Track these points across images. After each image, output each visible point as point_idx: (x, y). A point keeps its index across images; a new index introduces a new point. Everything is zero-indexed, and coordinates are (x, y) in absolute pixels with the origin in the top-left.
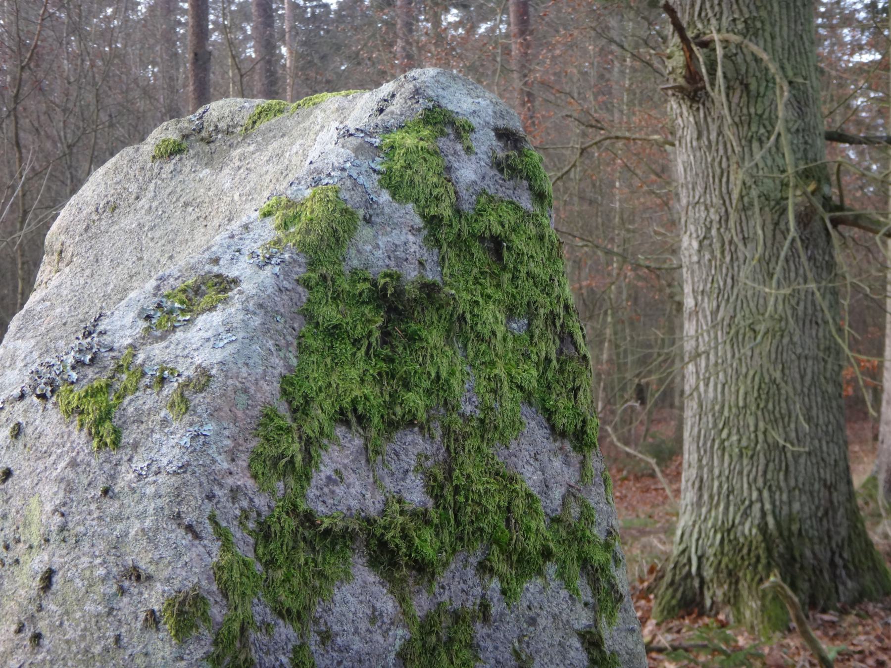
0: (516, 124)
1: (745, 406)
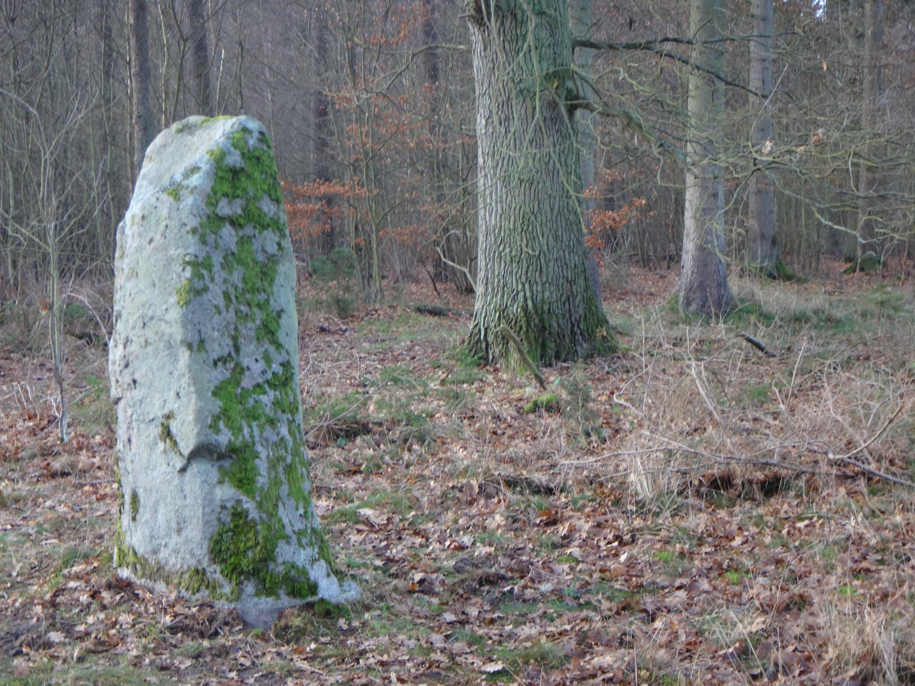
0: (264, 130)
1: (514, 229)
